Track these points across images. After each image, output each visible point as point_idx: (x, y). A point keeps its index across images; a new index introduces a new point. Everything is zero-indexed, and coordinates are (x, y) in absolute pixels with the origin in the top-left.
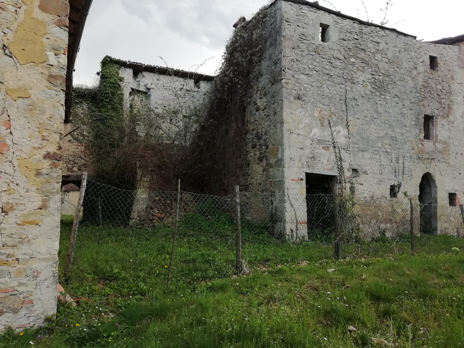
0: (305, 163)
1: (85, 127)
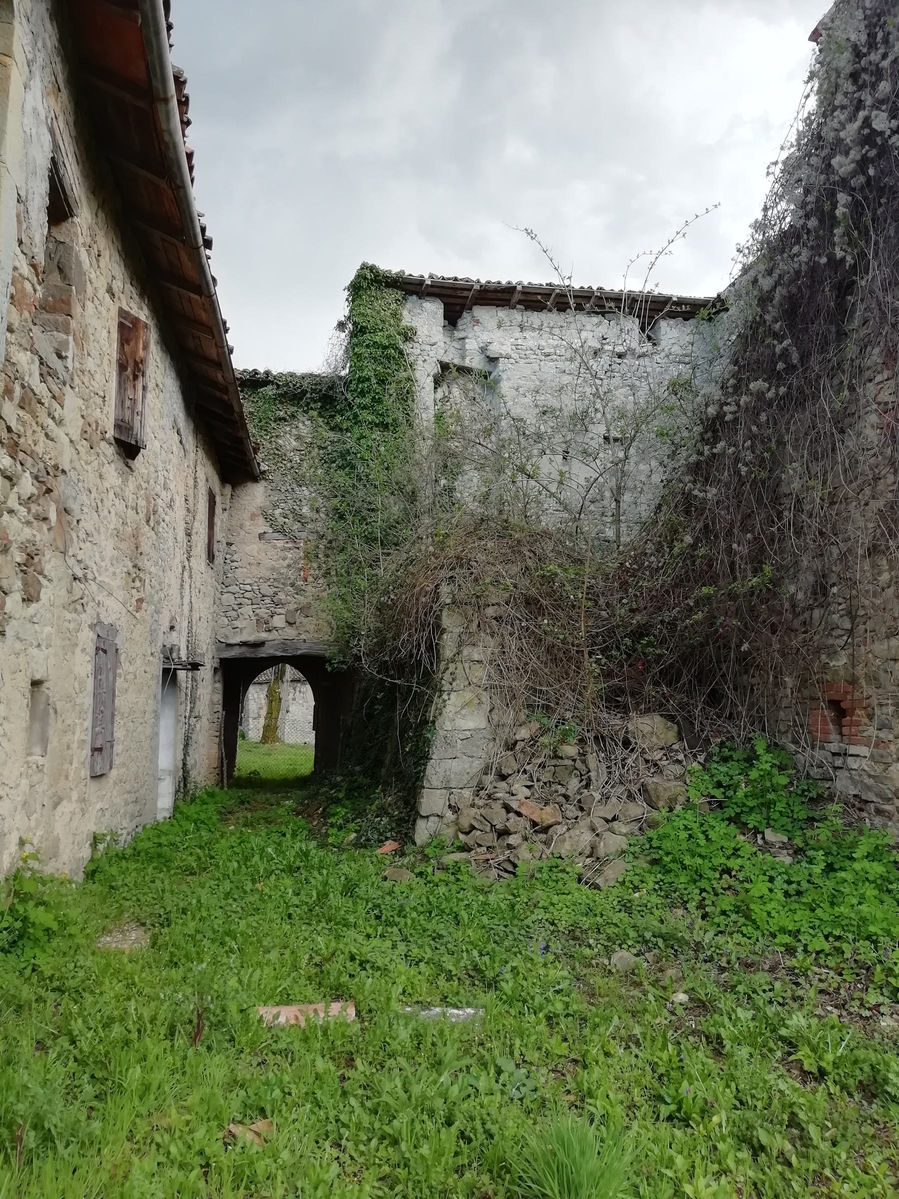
1: (306, 493)
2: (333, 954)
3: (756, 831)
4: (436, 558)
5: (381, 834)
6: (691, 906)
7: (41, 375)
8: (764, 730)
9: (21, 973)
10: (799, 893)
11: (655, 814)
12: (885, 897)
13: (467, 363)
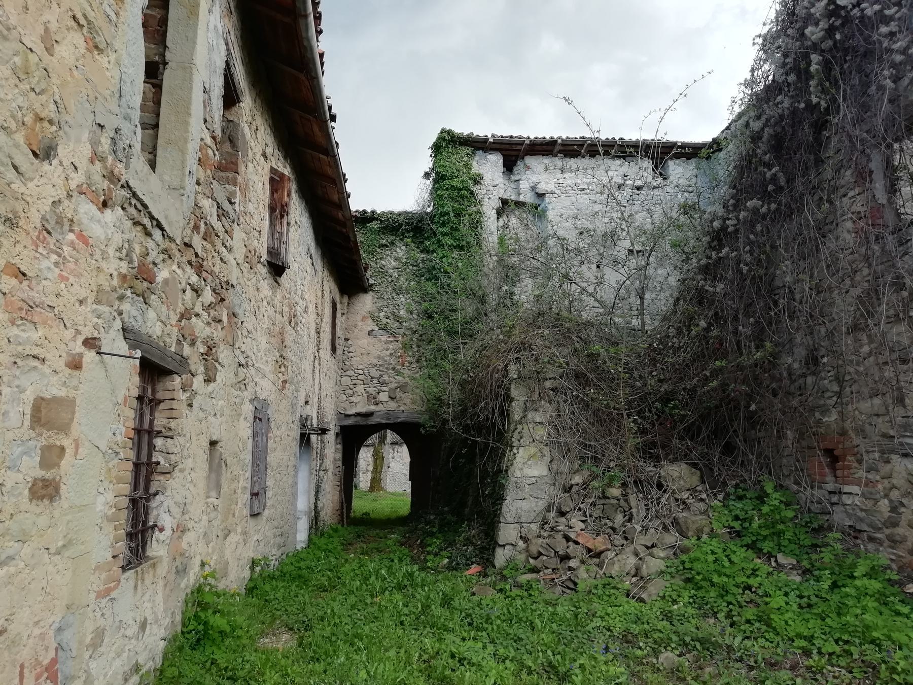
1: (403, 299)
2: (438, 653)
3: (770, 556)
4: (506, 344)
5: (468, 560)
6: (721, 616)
7: (218, 215)
8: (771, 475)
9: (204, 666)
10: (810, 606)
11: (686, 542)
12: (884, 609)
13: (522, 198)
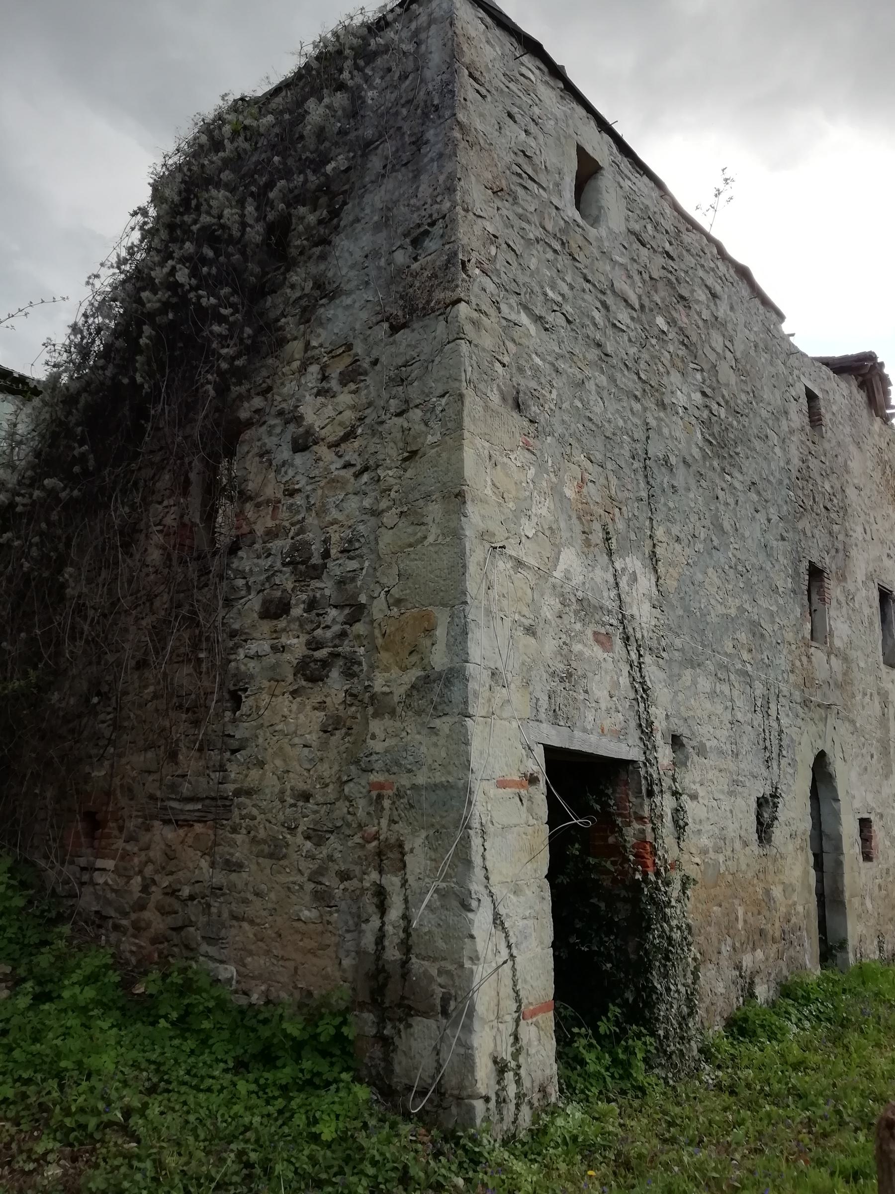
0: (544, 702)
